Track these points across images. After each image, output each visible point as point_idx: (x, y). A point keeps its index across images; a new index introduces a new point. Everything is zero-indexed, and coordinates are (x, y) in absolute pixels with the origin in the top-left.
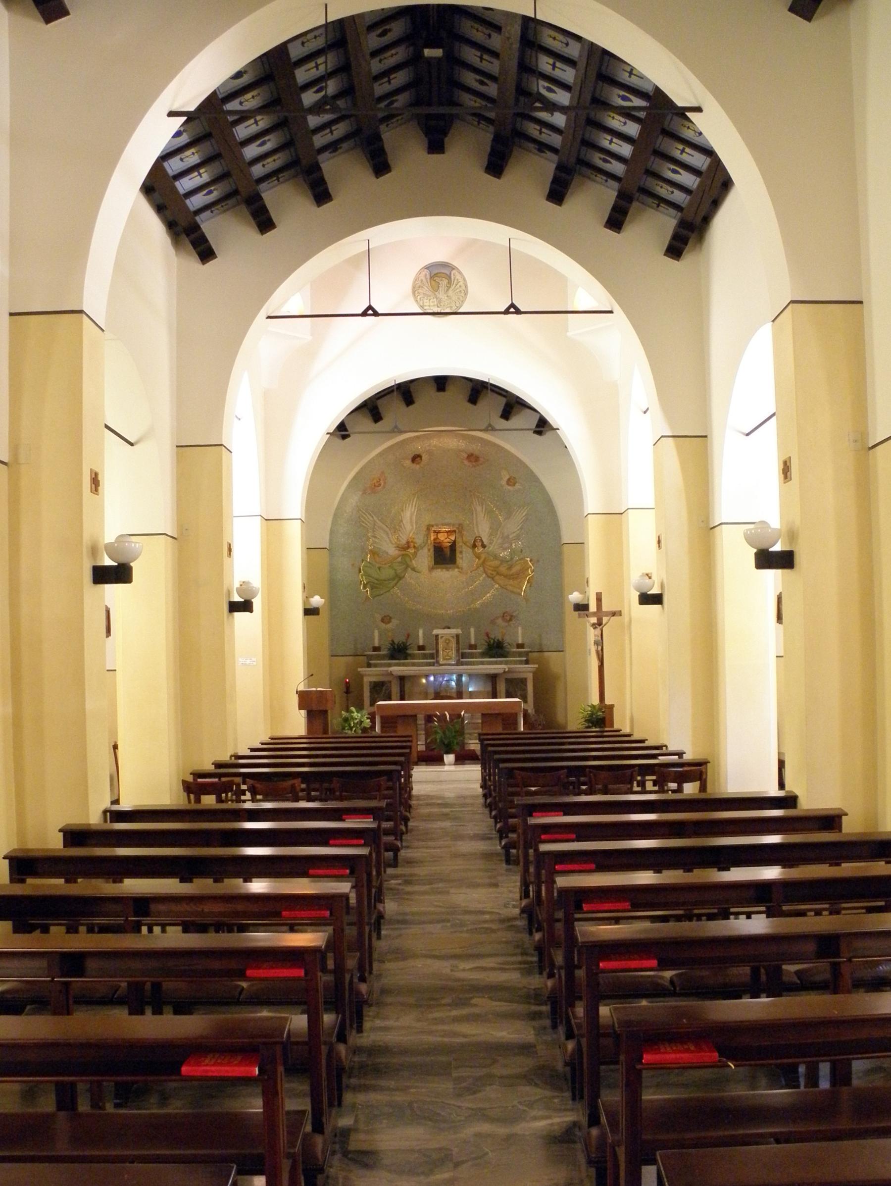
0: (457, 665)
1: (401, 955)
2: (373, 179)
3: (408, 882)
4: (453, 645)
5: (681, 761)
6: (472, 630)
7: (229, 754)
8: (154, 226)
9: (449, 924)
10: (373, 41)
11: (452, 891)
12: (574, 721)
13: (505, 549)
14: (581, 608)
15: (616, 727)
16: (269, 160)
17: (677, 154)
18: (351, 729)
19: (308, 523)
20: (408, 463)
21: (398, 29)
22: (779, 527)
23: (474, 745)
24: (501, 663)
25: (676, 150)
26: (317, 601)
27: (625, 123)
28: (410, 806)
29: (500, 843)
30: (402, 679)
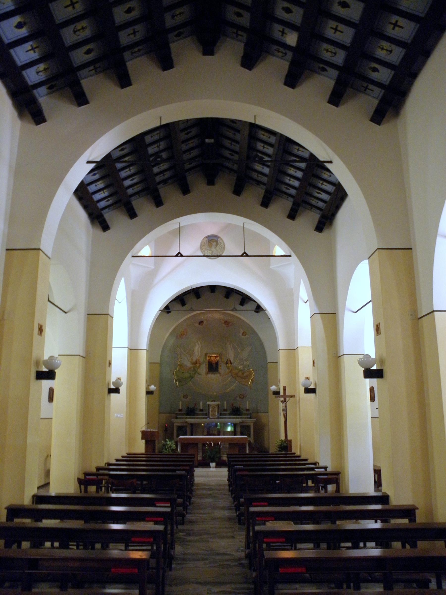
0: (218, 418)
1: (183, 581)
2: (181, 195)
3: (189, 535)
4: (216, 409)
5: (326, 472)
6: (225, 403)
7: (104, 463)
8: (81, 214)
9: (208, 561)
10: (183, 136)
11: (210, 540)
12: (273, 449)
13: (241, 365)
14: (276, 393)
15: (293, 451)
16: (136, 187)
17: (320, 185)
18: (166, 449)
19: (150, 351)
20: (197, 324)
21: (194, 131)
22: (374, 357)
23: (225, 458)
24: (238, 418)
25: (320, 184)
26: (152, 387)
27: (296, 172)
28: (192, 491)
29: (236, 513)
30: (192, 425)
